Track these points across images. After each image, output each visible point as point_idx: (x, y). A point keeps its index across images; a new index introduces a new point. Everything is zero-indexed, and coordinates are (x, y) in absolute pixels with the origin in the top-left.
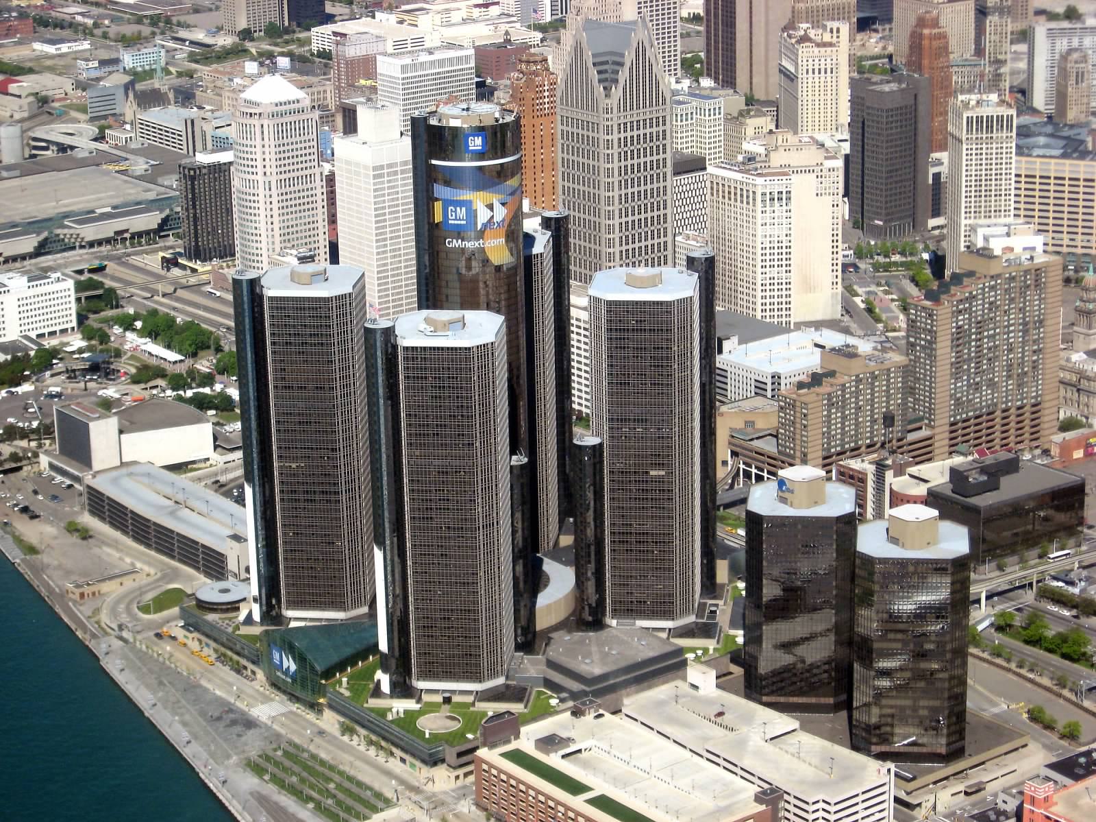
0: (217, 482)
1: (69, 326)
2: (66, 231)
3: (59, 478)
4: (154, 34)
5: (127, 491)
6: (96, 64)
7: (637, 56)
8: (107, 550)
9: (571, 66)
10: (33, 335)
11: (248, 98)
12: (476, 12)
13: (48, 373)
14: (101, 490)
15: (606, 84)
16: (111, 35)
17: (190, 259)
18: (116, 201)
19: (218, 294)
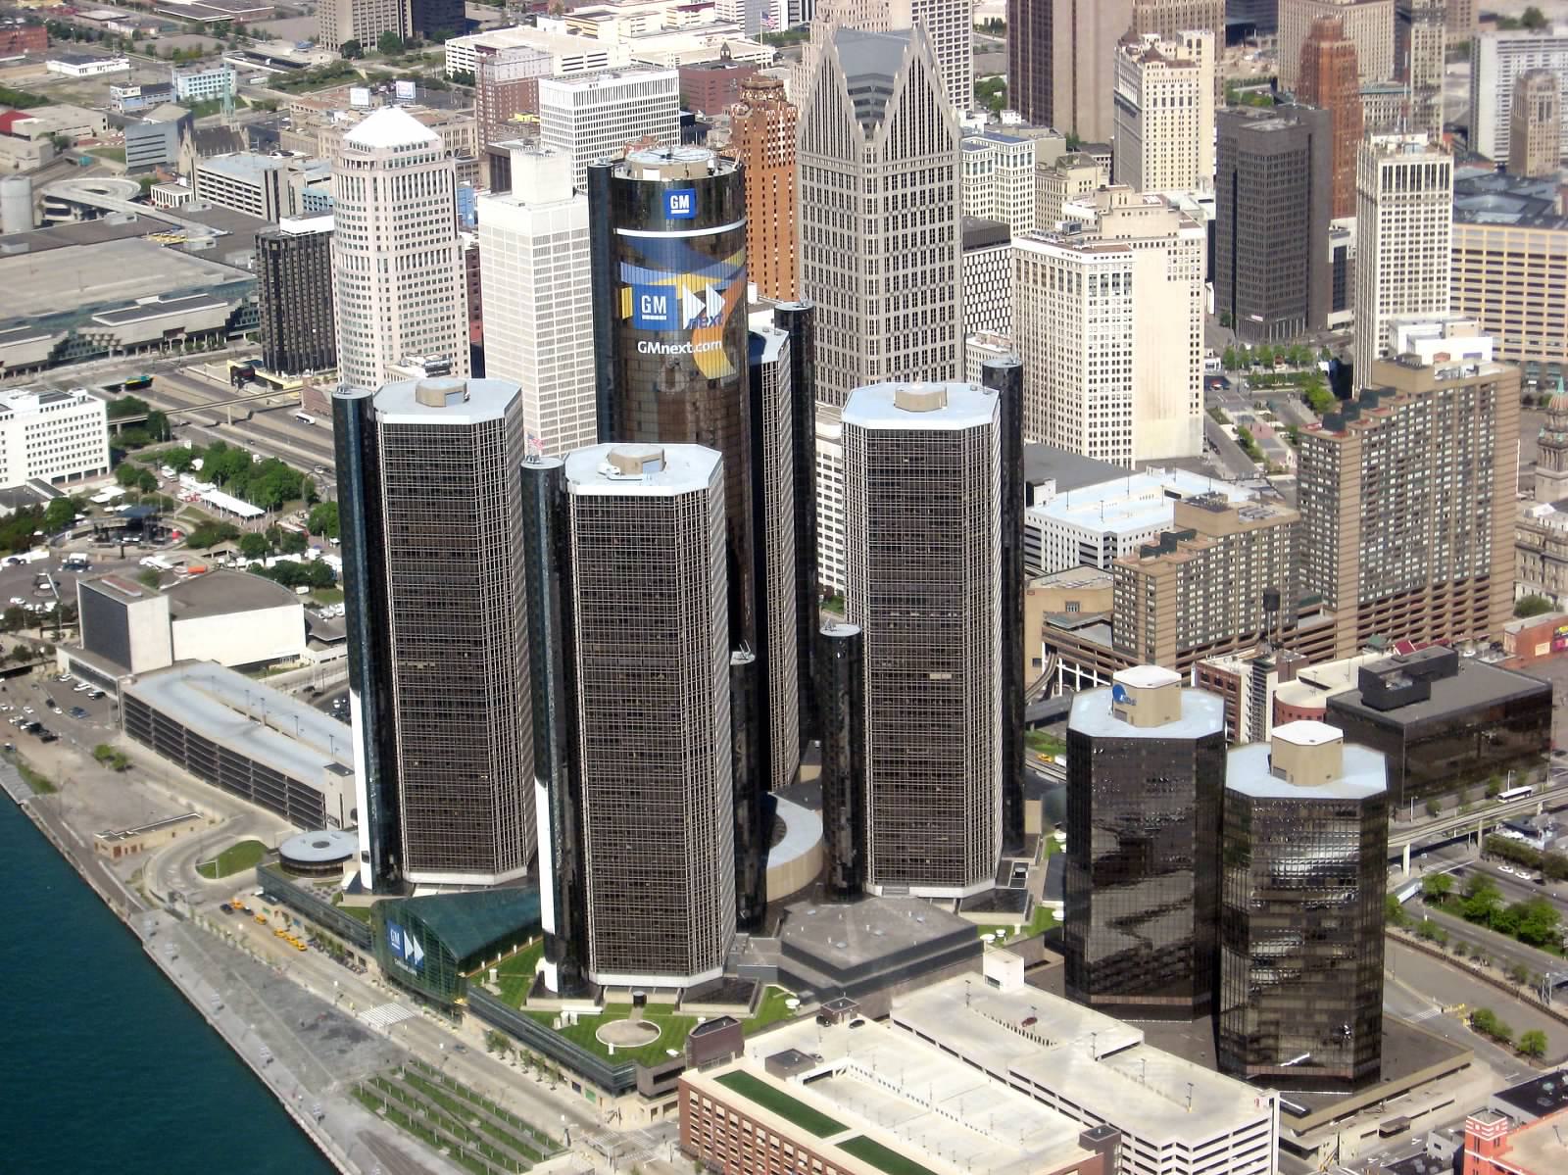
0: (311, 688)
1: (98, 466)
2: (94, 330)
3: (84, 684)
4: (220, 48)
5: (181, 702)
6: (137, 91)
7: (912, 80)
8: (153, 786)
9: (817, 94)
10: (47, 478)
11: (355, 140)
12: (681, 18)
13: (69, 534)
14: (144, 700)
15: (867, 120)
16: (159, 50)
17: (272, 371)
18: (166, 288)
19: (312, 420)
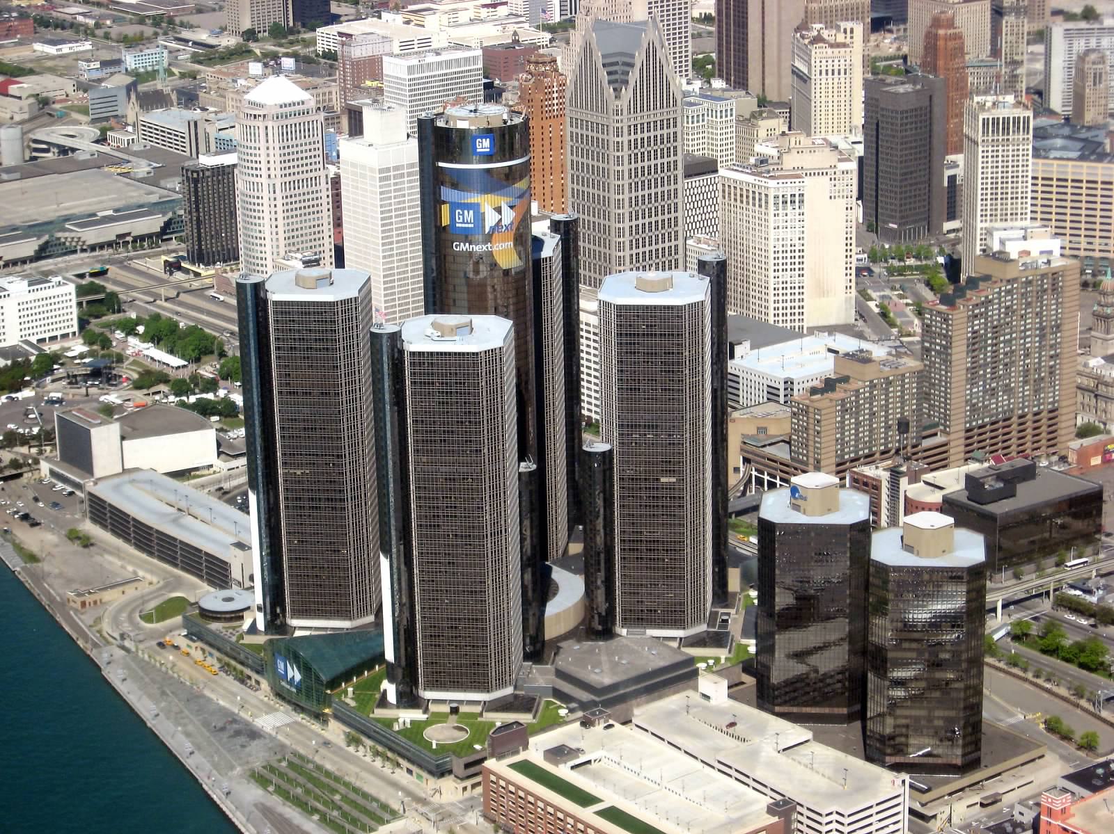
0: (221, 489)
1: (70, 330)
2: (67, 234)
3: (60, 485)
4: (156, 34)
5: (129, 498)
6: (98, 65)
7: (648, 57)
8: (109, 558)
9: (580, 67)
10: (34, 340)
11: (252, 99)
12: (484, 13)
13: (49, 379)
14: (102, 497)
15: (616, 85)
16: (113, 36)
17: (193, 263)
18: (118, 204)
19: (222, 298)
